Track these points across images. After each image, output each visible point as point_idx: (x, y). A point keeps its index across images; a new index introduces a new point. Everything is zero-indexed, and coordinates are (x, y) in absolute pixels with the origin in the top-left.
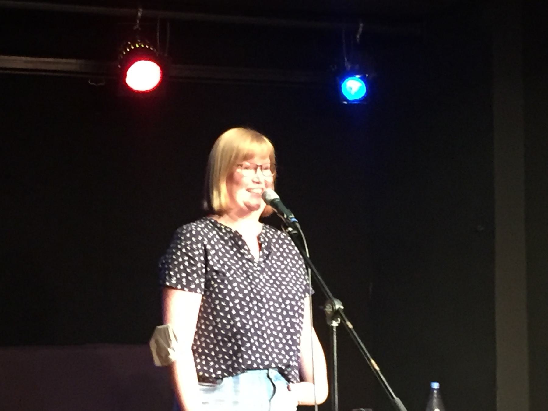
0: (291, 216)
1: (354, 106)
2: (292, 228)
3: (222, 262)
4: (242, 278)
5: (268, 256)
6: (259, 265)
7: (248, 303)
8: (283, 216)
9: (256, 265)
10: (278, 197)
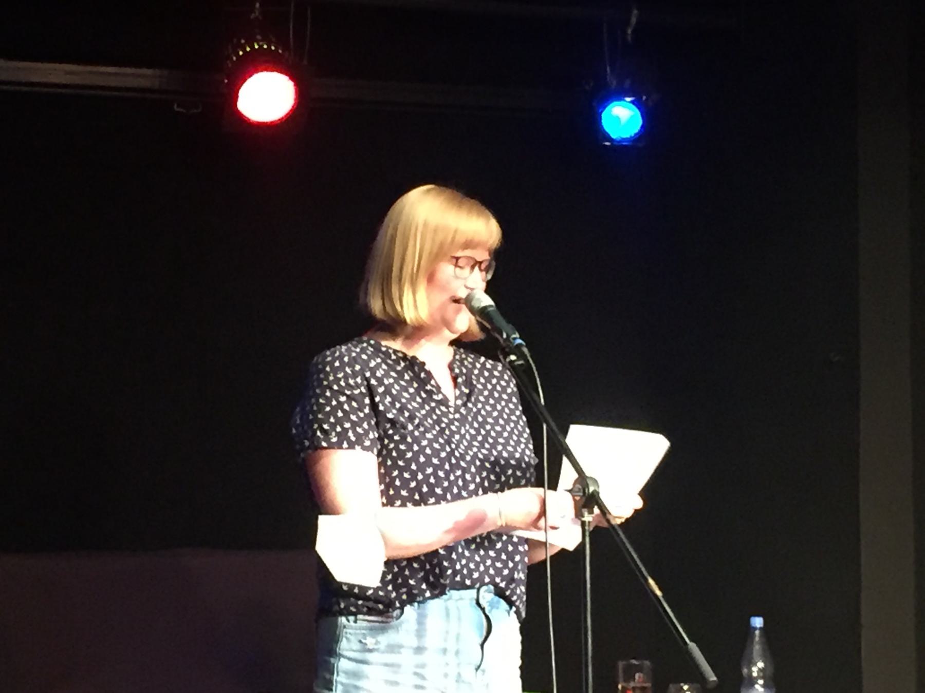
0: (514, 336)
1: (622, 148)
2: (515, 355)
3: (398, 405)
4: (434, 432)
5: (469, 396)
6: (457, 410)
7: (447, 474)
8: (502, 336)
9: (452, 410)
10: (491, 302)
